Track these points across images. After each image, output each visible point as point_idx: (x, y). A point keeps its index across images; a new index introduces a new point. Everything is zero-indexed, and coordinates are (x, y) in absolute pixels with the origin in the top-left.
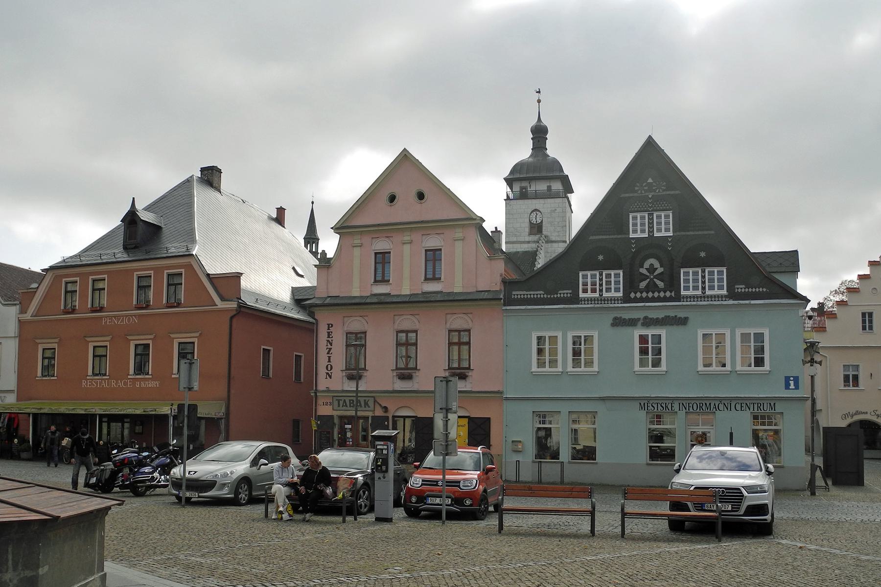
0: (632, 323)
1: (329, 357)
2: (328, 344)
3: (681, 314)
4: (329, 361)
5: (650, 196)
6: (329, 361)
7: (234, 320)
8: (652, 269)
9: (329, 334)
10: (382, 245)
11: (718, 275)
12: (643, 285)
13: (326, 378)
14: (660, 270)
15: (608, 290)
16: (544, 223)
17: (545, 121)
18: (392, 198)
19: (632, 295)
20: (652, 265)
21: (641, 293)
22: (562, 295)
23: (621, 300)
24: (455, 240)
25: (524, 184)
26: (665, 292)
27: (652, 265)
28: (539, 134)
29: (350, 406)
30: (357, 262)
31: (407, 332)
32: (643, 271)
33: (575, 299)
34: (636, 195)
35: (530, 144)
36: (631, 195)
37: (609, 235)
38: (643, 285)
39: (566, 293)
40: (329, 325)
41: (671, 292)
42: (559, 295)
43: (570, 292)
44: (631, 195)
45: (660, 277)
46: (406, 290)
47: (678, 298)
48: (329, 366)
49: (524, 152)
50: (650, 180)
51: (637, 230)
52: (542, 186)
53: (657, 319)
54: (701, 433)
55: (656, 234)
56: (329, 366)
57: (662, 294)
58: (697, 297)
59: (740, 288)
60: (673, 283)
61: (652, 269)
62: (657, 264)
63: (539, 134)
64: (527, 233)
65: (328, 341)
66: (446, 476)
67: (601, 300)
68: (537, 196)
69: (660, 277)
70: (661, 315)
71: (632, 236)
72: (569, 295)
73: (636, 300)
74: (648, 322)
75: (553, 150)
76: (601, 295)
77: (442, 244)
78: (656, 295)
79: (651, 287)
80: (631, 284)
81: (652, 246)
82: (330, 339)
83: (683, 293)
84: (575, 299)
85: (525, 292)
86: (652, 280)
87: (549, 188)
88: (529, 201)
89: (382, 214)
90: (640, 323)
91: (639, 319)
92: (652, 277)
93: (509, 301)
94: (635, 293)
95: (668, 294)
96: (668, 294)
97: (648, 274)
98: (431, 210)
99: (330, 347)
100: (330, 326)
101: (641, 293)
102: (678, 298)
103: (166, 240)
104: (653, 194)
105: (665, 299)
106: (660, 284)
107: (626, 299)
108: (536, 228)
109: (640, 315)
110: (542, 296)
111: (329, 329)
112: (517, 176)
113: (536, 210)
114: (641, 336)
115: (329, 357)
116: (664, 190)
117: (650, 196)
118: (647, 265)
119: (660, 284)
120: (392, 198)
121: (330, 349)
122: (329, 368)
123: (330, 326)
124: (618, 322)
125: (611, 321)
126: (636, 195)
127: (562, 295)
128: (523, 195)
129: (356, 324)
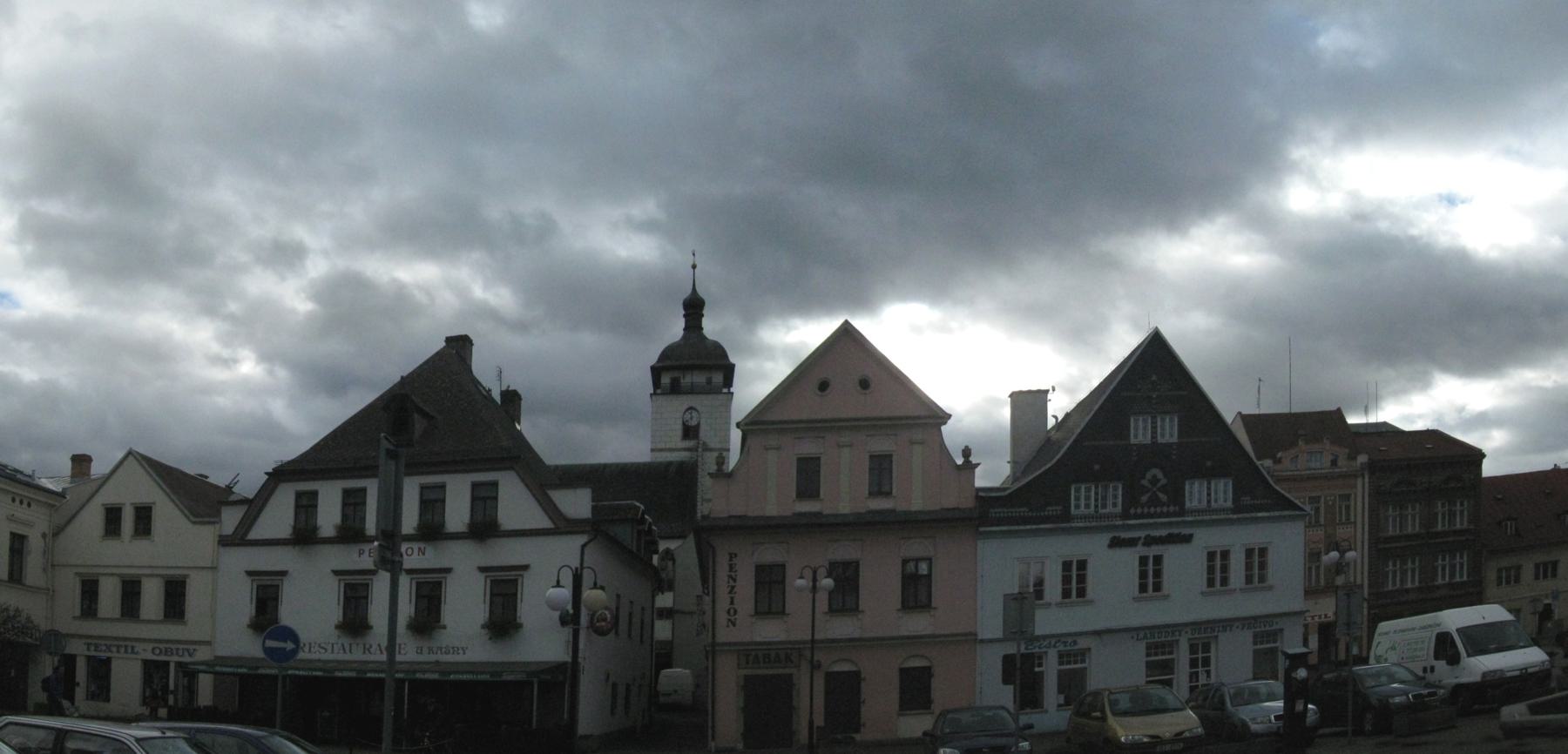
0: (1131, 543)
1: (732, 599)
2: (731, 581)
3: (1186, 531)
4: (732, 603)
5: (1154, 396)
6: (732, 603)
7: (587, 551)
8: (1155, 481)
9: (731, 567)
10: (808, 448)
11: (1223, 491)
12: (1144, 499)
13: (728, 626)
14: (1164, 481)
15: (1104, 506)
17: (701, 292)
18: (824, 386)
19: (1132, 511)
20: (1154, 476)
21: (1143, 508)
22: (1050, 513)
23: (1120, 517)
24: (767, 449)
25: (676, 374)
26: (1168, 506)
27: (1154, 476)
29: (764, 662)
31: (917, 560)
32: (1145, 482)
35: (681, 323)
38: (1144, 499)
40: (730, 554)
41: (1175, 506)
42: (1046, 513)
43: (1060, 508)
45: (1163, 489)
46: (845, 508)
47: (1182, 512)
48: (732, 611)
49: (675, 329)
50: (1154, 378)
51: (1140, 432)
52: (699, 378)
53: (1161, 537)
54: (1037, 669)
55: (1160, 440)
56: (732, 611)
57: (1165, 509)
58: (1202, 512)
59: (1246, 500)
60: (1177, 497)
61: (1155, 481)
62: (1160, 475)
65: (730, 577)
66: (1282, 705)
67: (1097, 518)
68: (693, 390)
69: (1163, 489)
70: (1163, 532)
71: (1133, 441)
72: (1059, 512)
73: (1137, 516)
74: (1150, 541)
75: (711, 327)
76: (1096, 512)
77: (822, 450)
78: (1159, 510)
79: (1155, 501)
80: (1131, 500)
81: (1155, 453)
82: (733, 574)
83: (1188, 505)
84: (1066, 516)
85: (1000, 510)
86: (1155, 492)
87: (709, 381)
88: (684, 398)
89: (809, 407)
90: (1140, 542)
91: (1140, 538)
92: (1155, 489)
94: (1136, 508)
95: (1172, 509)
96: (1172, 509)
97: (1150, 486)
99: (733, 584)
100: (732, 556)
101: (1143, 508)
102: (1182, 512)
103: (1141, 424)
105: (1168, 515)
106: (1163, 497)
107: (1125, 515)
108: (690, 432)
109: (1142, 534)
110: (1026, 514)
111: (731, 560)
112: (668, 363)
113: (691, 408)
114: (760, 569)
115: (732, 599)
117: (1154, 396)
118: (1149, 476)
119: (1163, 497)
120: (824, 386)
121: (733, 587)
122: (732, 612)
123: (732, 556)
124: (1116, 543)
125: (1108, 542)
127: (1050, 513)
128: (675, 389)
129: (770, 554)
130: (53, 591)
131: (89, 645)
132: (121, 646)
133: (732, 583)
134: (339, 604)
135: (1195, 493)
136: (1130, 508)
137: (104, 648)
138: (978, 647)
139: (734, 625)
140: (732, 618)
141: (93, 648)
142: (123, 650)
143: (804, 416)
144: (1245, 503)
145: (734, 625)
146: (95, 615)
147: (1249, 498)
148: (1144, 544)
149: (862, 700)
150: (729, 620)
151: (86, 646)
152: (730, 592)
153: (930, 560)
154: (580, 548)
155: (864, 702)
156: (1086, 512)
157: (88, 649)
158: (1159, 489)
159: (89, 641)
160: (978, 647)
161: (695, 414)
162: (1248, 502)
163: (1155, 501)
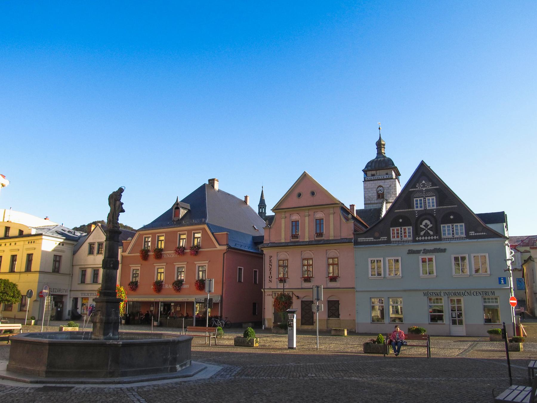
0: (418, 252)
1: (271, 272)
4: (270, 274)
5: (424, 190)
6: (270, 274)
8: (426, 226)
14: (431, 226)
16: (385, 193)
18: (299, 195)
20: (426, 223)
21: (422, 237)
22: (384, 239)
23: (412, 241)
26: (434, 236)
28: (380, 145)
30: (283, 225)
32: (422, 226)
33: (388, 242)
34: (417, 189)
36: (415, 189)
37: (405, 209)
39: (385, 238)
40: (270, 256)
43: (386, 238)
44: (415, 189)
45: (431, 229)
47: (440, 239)
48: (270, 277)
50: (424, 182)
55: (428, 208)
56: (270, 277)
57: (432, 238)
58: (450, 239)
59: (472, 233)
61: (426, 226)
63: (380, 145)
64: (376, 199)
69: (431, 229)
72: (386, 239)
78: (429, 238)
79: (427, 234)
80: (417, 232)
81: (426, 214)
85: (364, 239)
89: (294, 202)
92: (427, 229)
93: (356, 243)
95: (435, 237)
96: (435, 237)
98: (318, 200)
101: (422, 237)
104: (425, 188)
106: (431, 233)
110: (372, 240)
111: (270, 258)
115: (271, 272)
116: (431, 187)
117: (424, 190)
118: (424, 223)
119: (431, 233)
120: (299, 195)
121: (271, 268)
126: (417, 189)
130: (72, 275)
131: (82, 293)
132: (92, 293)
133: (271, 267)
134: (276, 218)
135: (446, 229)
136: (416, 237)
137: (87, 294)
138: (356, 293)
139: (271, 282)
140: (271, 279)
141: (83, 295)
142: (92, 295)
143: (491, 288)
144: (472, 234)
145: (271, 282)
146: (85, 283)
147: (474, 232)
148: (423, 253)
149: (314, 321)
150: (270, 280)
151: (81, 294)
152: (270, 270)
153: (338, 258)
154: (223, 254)
155: (315, 322)
156: (397, 239)
157: (82, 295)
158: (428, 229)
159: (82, 292)
160: (356, 293)
161: (381, 188)
162: (474, 234)
163: (427, 234)
